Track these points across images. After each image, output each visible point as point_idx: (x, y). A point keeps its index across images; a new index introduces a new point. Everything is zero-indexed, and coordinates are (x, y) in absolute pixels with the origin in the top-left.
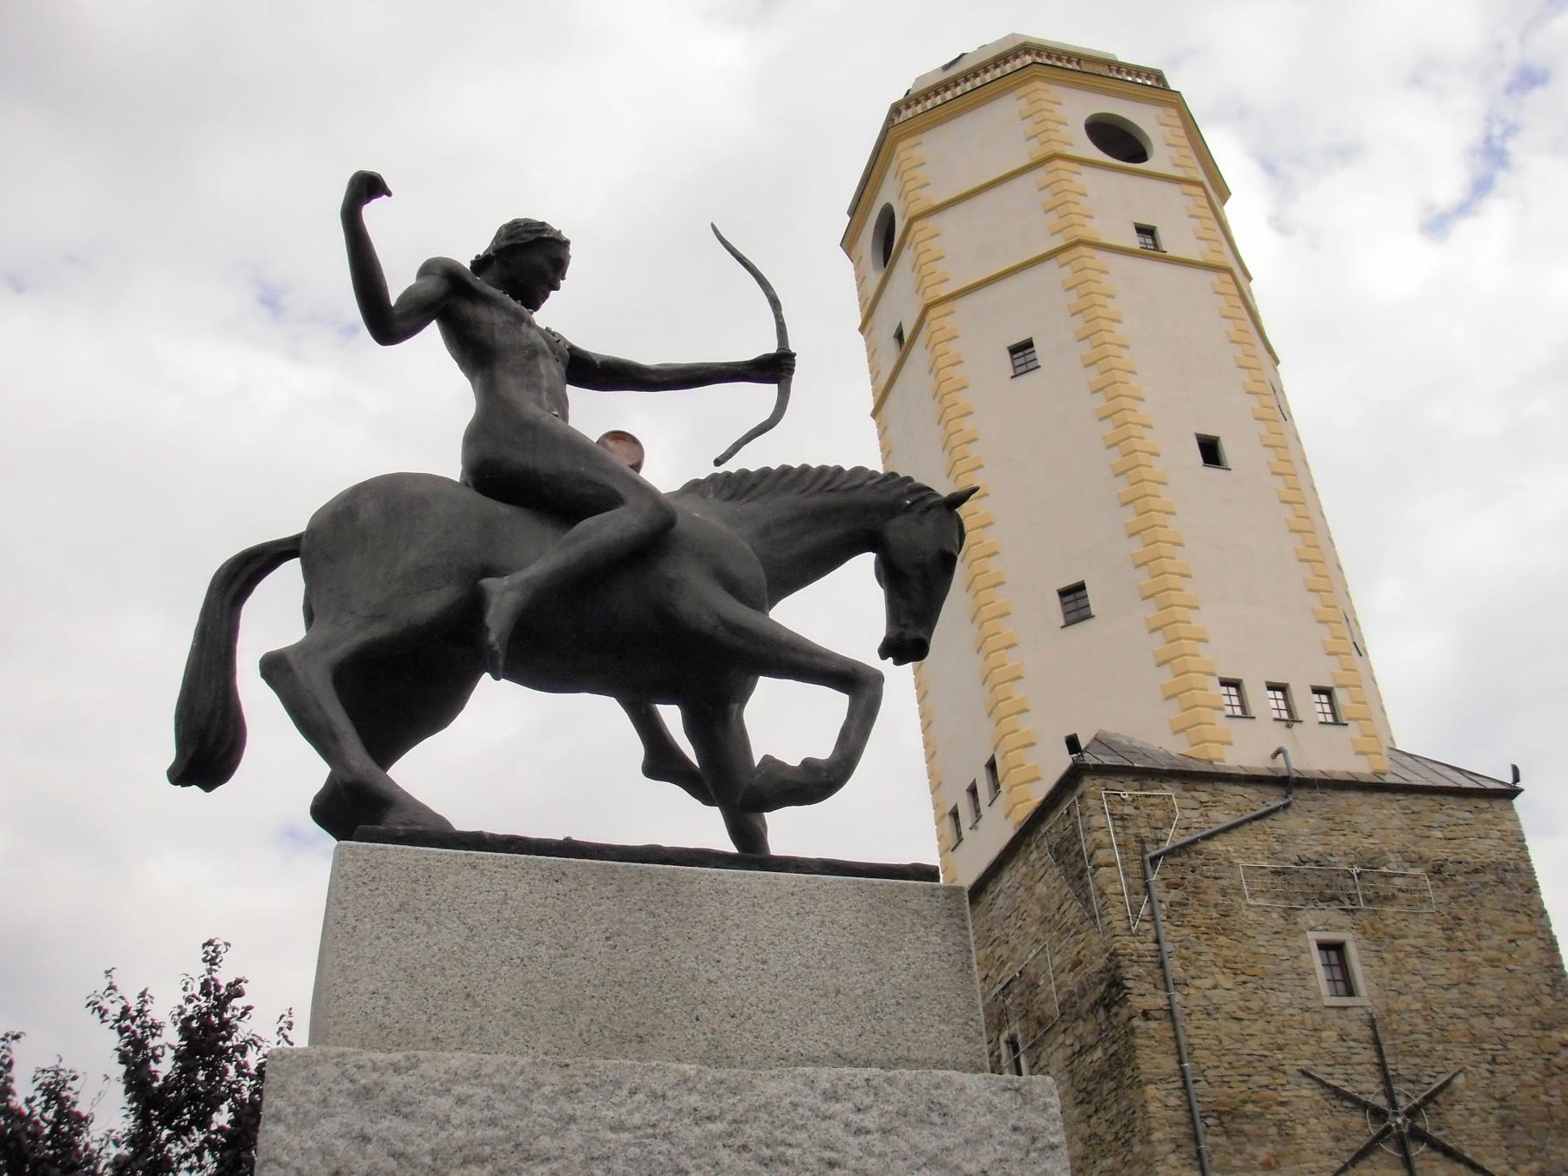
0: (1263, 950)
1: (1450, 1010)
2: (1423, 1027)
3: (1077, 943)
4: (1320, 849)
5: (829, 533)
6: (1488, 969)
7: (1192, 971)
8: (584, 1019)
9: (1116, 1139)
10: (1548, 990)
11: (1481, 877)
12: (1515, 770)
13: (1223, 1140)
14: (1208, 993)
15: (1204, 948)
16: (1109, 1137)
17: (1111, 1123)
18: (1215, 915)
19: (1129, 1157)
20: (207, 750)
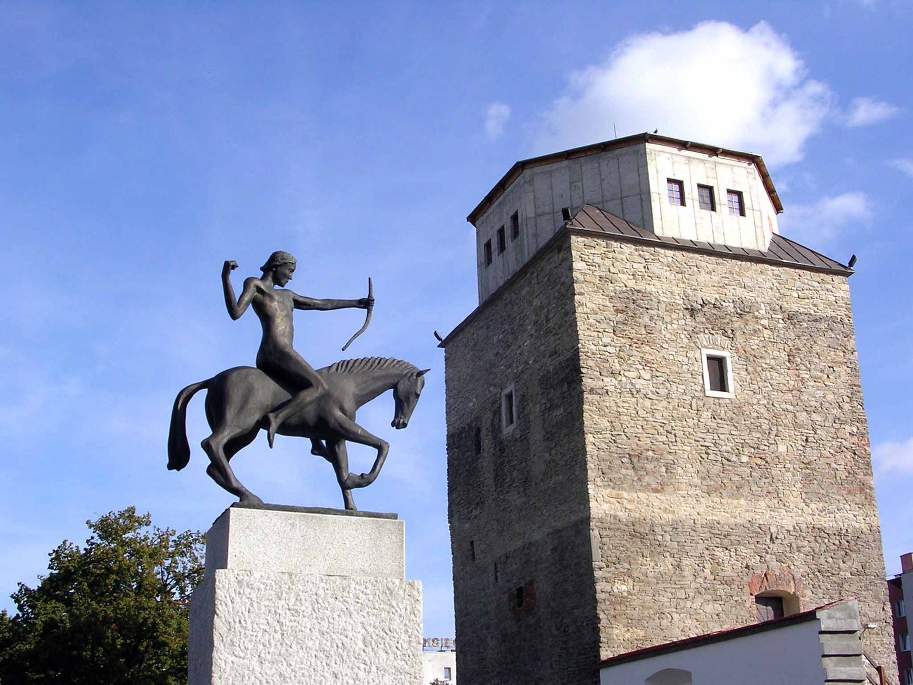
0: (671, 357)
1: (784, 406)
2: (766, 415)
3: (555, 340)
4: (717, 296)
5: (379, 384)
6: (813, 383)
7: (625, 367)
8: (295, 560)
9: (566, 464)
10: (848, 400)
11: (818, 325)
12: (853, 259)
13: (631, 472)
14: (633, 381)
15: (635, 353)
16: (562, 463)
17: (563, 455)
18: (644, 332)
19: (573, 476)
20: (178, 455)
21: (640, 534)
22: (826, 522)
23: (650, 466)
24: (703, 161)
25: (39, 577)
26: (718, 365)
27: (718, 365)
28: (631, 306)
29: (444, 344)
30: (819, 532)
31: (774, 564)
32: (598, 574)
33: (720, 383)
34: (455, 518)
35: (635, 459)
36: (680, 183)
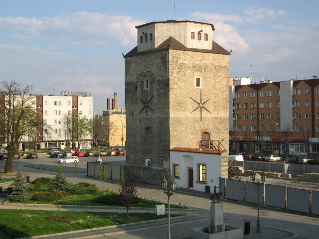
21: (179, 121)
22: (217, 116)
23: (182, 105)
24: (199, 26)
25: (180, 203)
26: (198, 80)
27: (198, 80)
28: (182, 66)
29: (125, 57)
30: (216, 118)
31: (206, 126)
32: (171, 130)
33: (198, 85)
34: (128, 104)
35: (179, 104)
36: (194, 33)
